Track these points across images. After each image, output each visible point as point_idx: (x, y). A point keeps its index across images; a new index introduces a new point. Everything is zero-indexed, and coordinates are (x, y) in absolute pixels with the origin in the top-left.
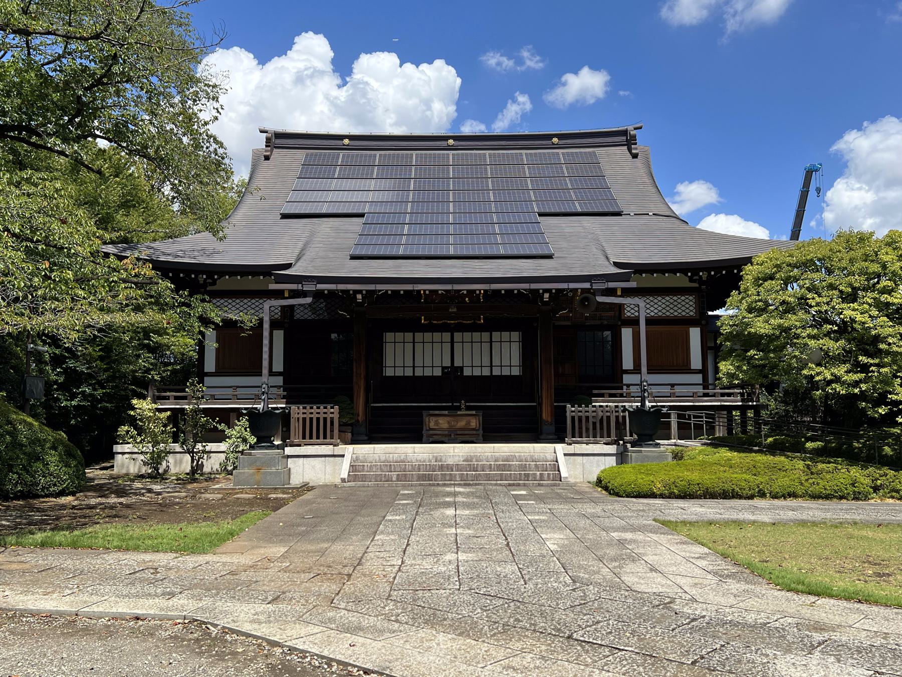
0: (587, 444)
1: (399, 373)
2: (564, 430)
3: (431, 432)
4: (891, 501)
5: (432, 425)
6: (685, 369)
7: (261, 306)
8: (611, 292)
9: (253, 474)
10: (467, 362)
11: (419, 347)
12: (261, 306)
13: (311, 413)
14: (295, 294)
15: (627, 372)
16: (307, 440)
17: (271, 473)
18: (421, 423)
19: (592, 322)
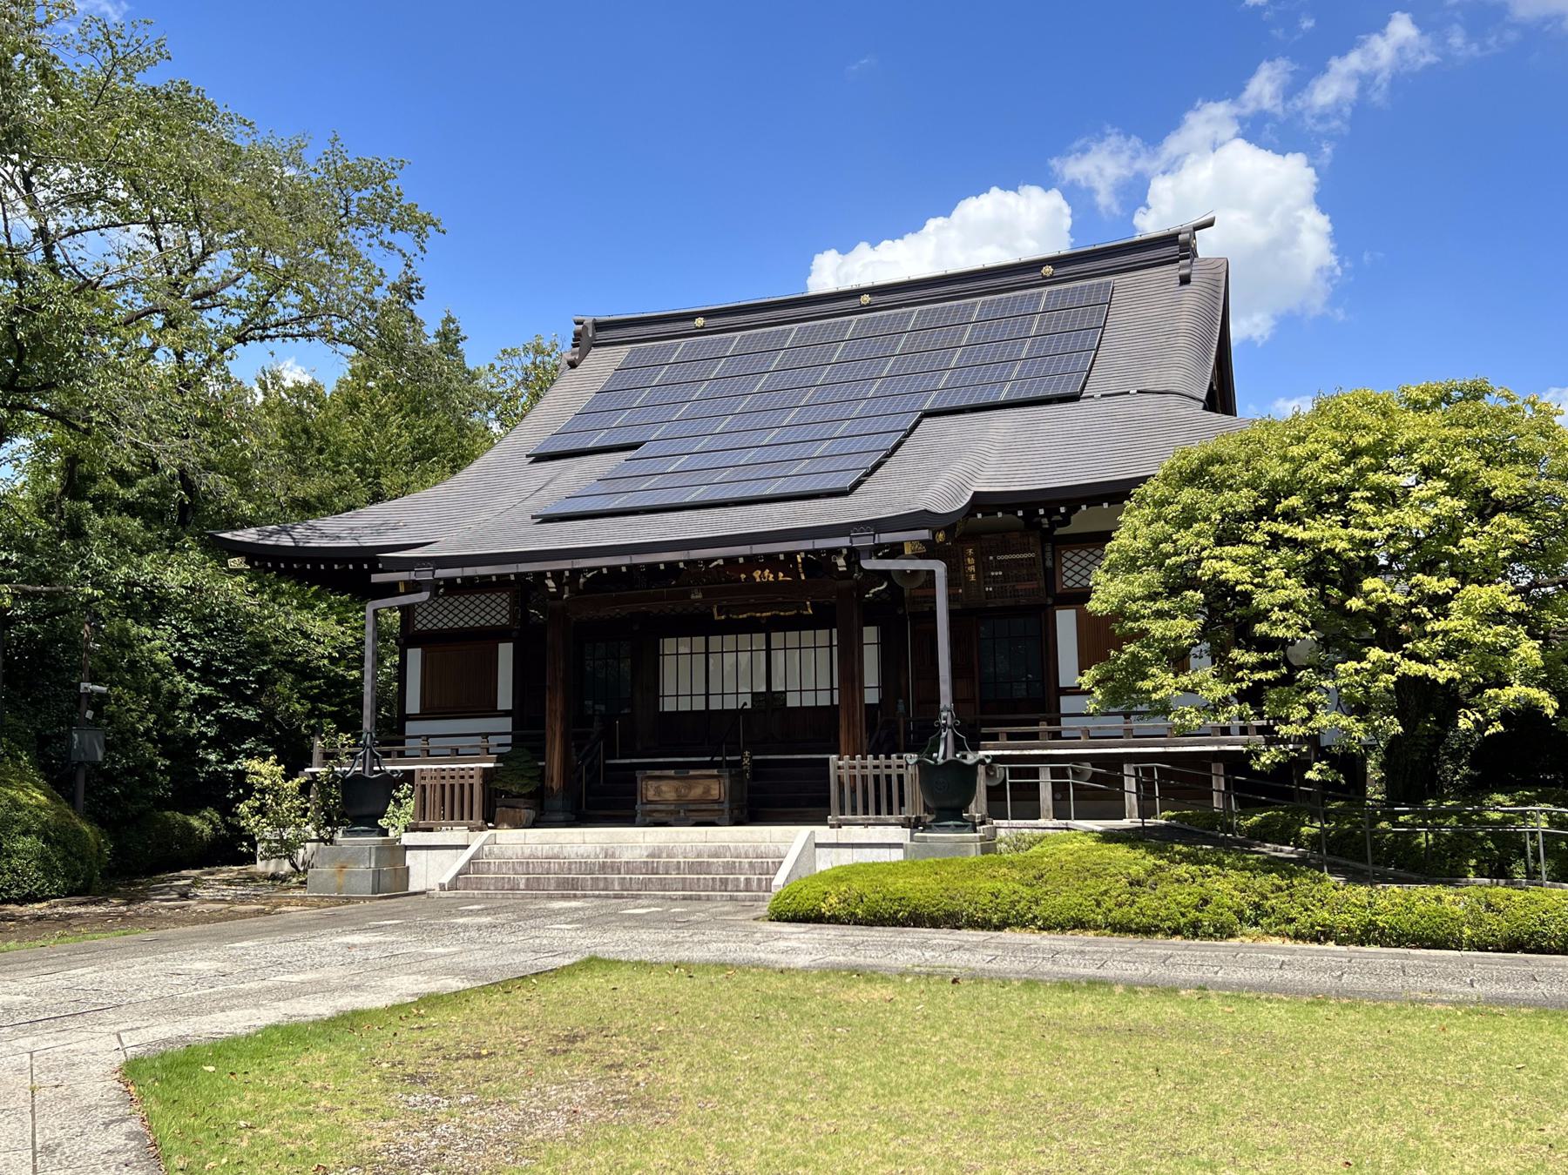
0: (866, 825)
1: (684, 706)
2: (826, 802)
3: (649, 807)
4: (1277, 941)
5: (651, 795)
6: (491, 711)
7: (1084, 572)
8: (895, 551)
9: (334, 875)
10: (794, 684)
11: (778, 657)
12: (1084, 572)
13: (888, 767)
14: (414, 587)
15: (414, 718)
16: (860, 817)
17: (357, 874)
18: (633, 793)
19: (998, 603)
